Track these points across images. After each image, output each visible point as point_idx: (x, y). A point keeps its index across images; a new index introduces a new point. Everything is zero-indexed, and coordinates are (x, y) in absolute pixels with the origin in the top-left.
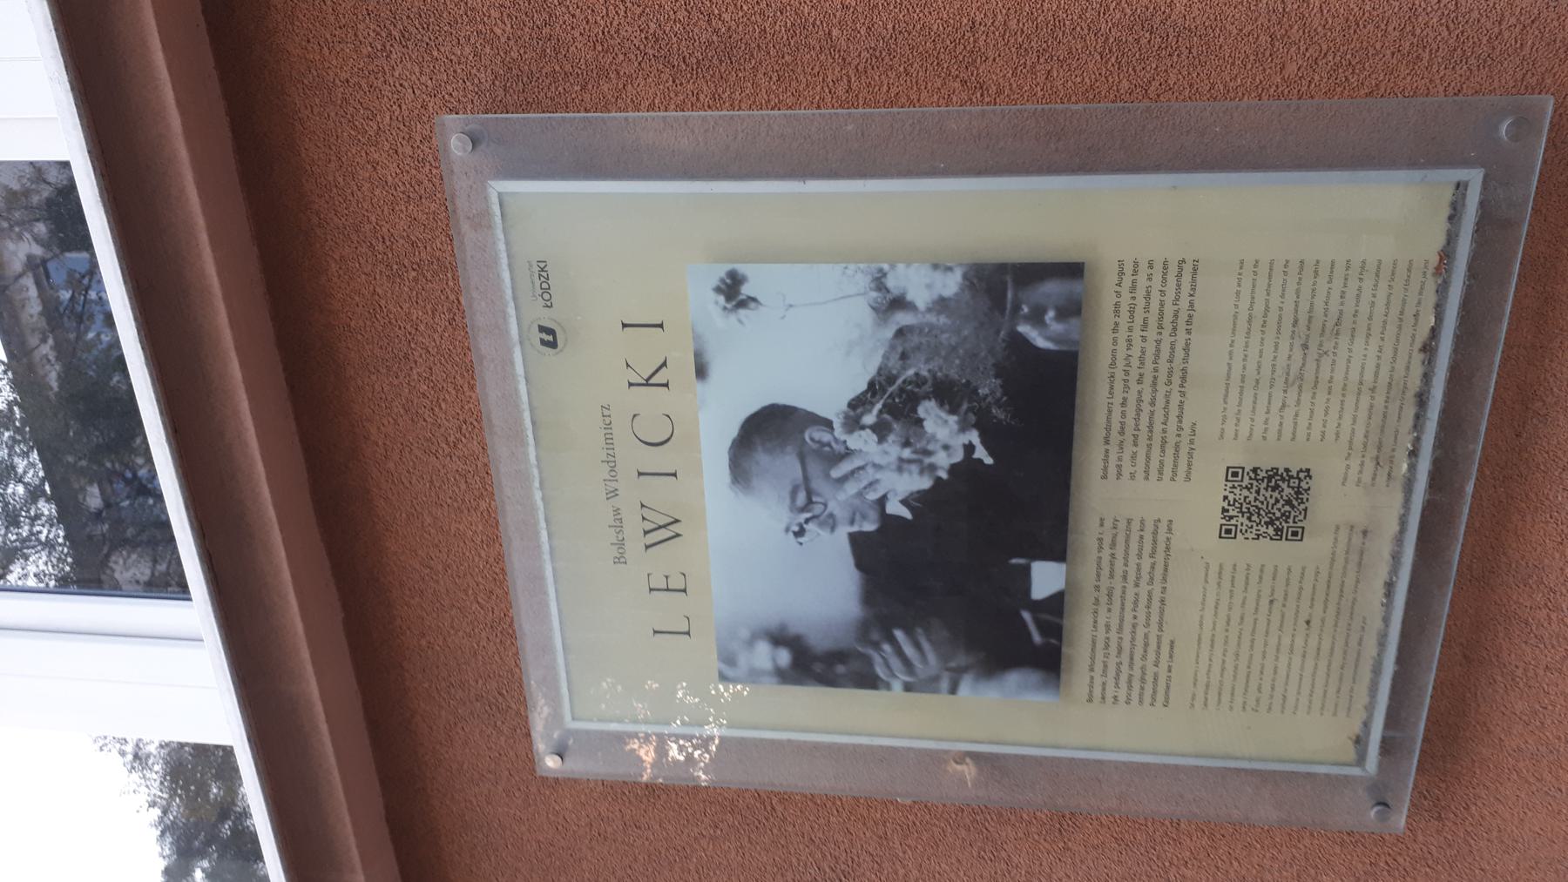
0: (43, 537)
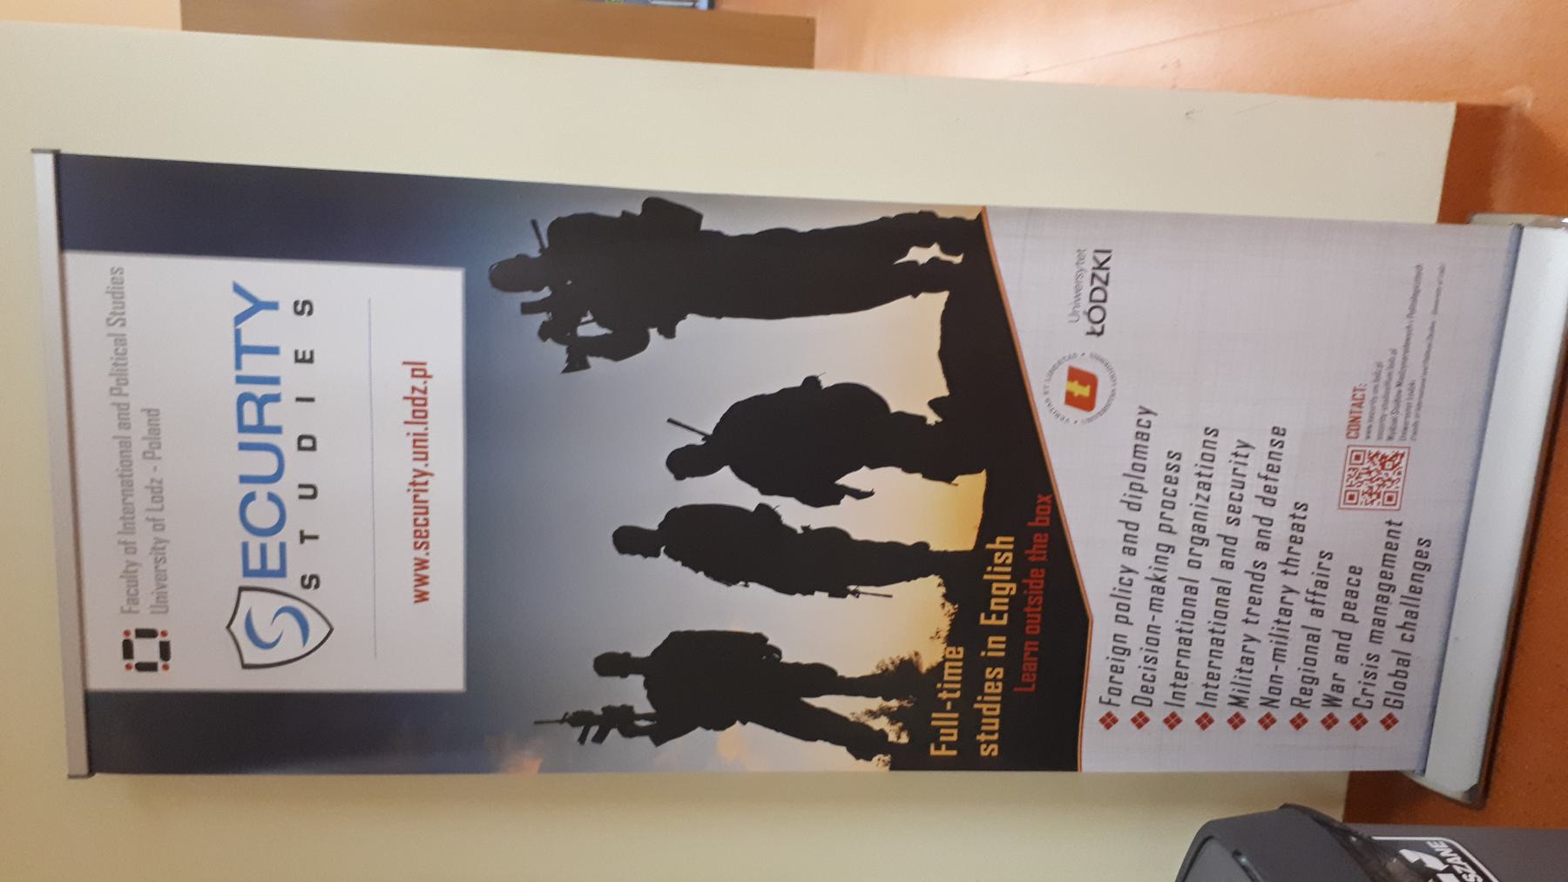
0: (1012, 588)
